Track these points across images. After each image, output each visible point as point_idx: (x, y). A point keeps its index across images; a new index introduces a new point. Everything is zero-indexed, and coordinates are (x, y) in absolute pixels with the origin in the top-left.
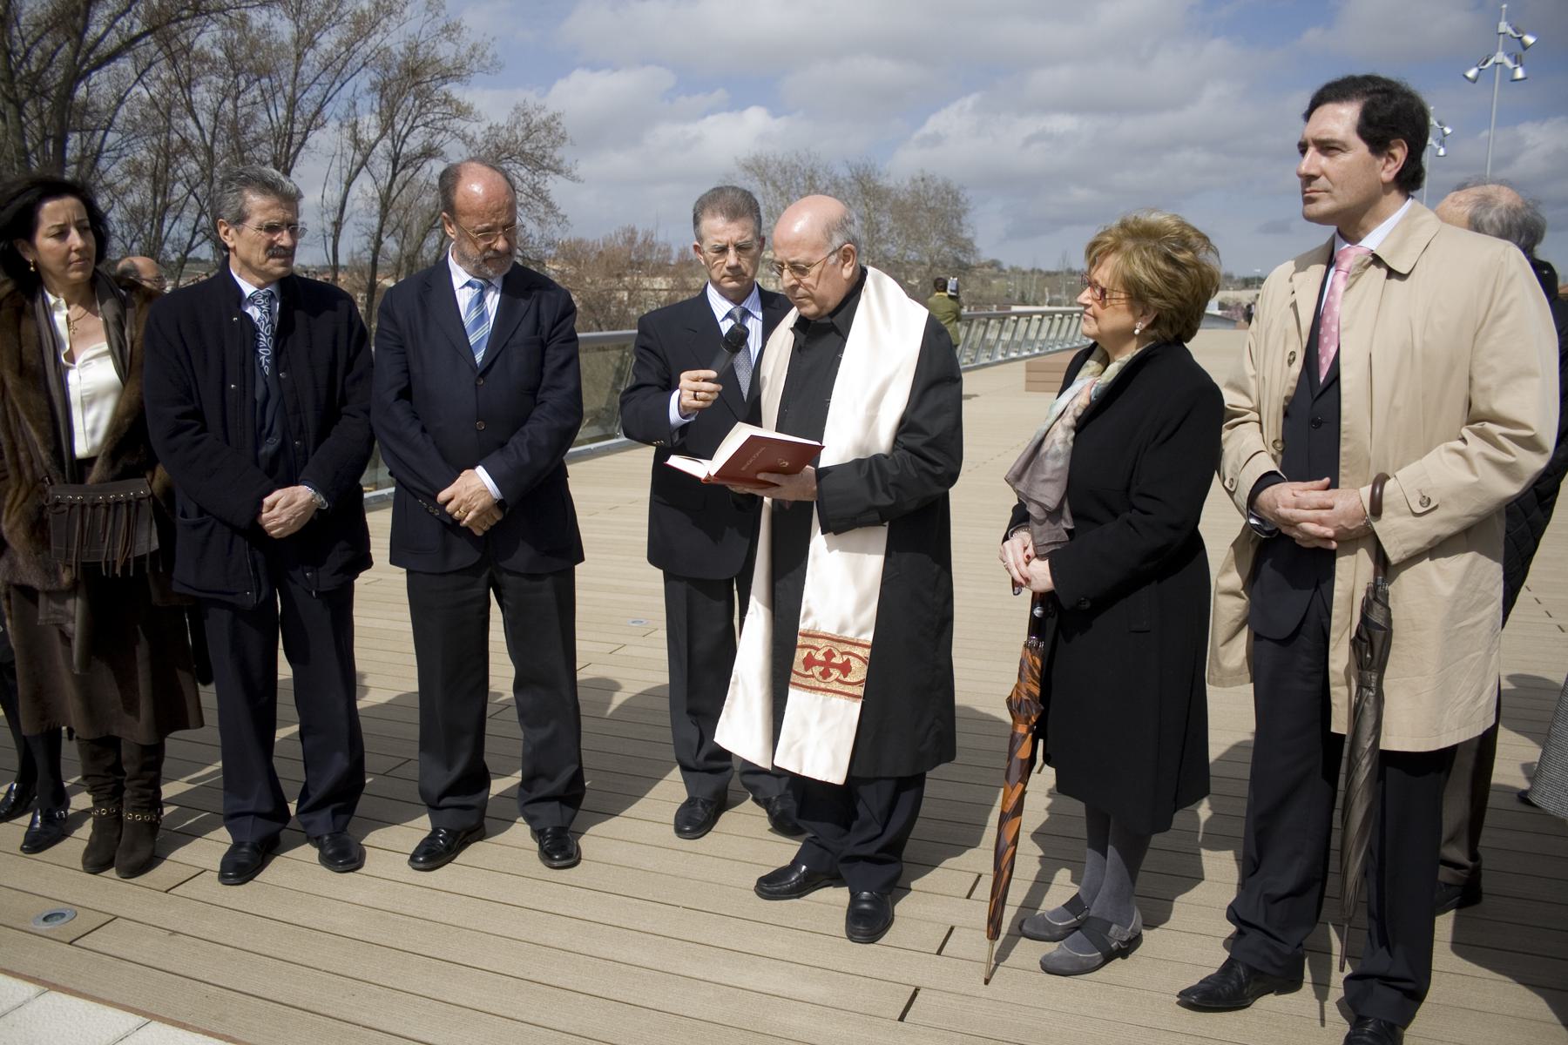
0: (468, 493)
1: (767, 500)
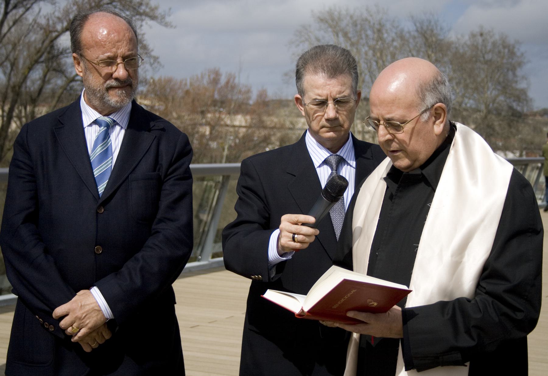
0: (83, 311)
1: (355, 335)
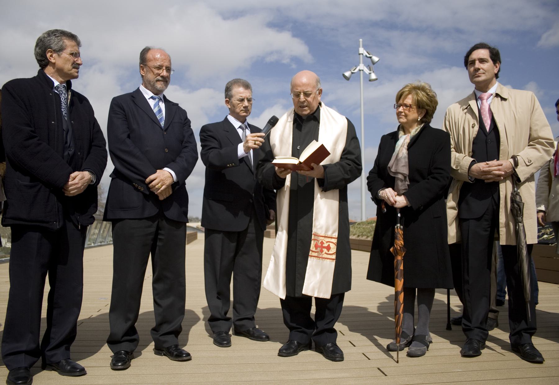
0: (164, 177)
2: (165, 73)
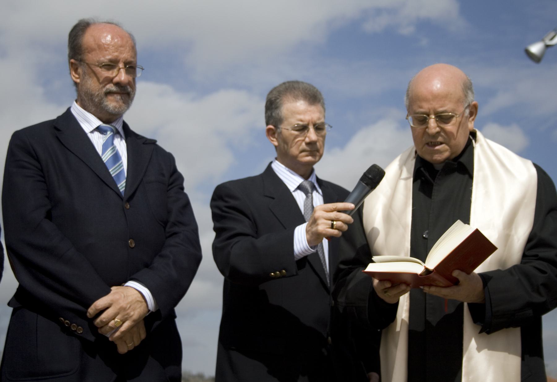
2: (123, 77)
